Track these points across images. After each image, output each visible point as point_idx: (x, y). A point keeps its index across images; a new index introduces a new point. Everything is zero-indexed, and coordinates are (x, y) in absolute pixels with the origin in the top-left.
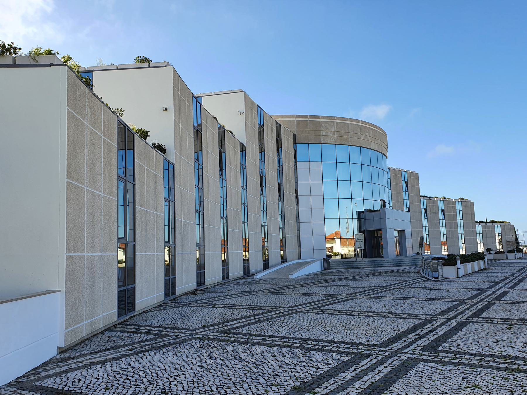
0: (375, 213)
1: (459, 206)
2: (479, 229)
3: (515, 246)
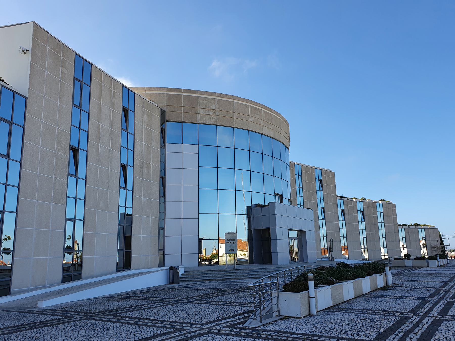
0: (263, 208)
1: (380, 208)
2: (402, 232)
3: (439, 251)
